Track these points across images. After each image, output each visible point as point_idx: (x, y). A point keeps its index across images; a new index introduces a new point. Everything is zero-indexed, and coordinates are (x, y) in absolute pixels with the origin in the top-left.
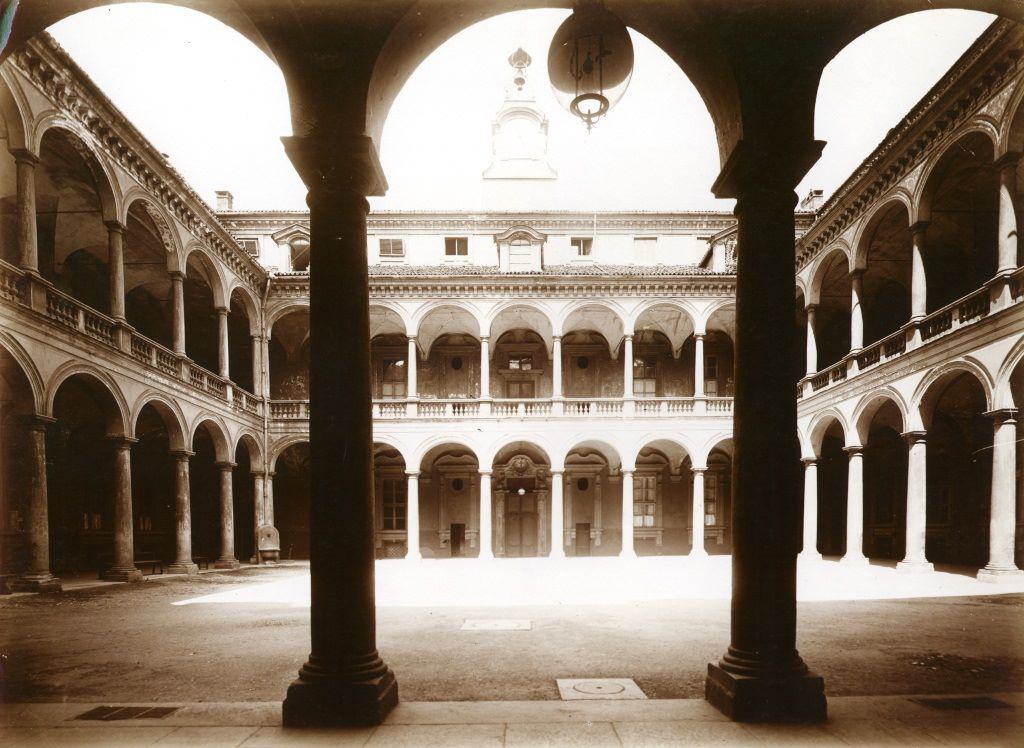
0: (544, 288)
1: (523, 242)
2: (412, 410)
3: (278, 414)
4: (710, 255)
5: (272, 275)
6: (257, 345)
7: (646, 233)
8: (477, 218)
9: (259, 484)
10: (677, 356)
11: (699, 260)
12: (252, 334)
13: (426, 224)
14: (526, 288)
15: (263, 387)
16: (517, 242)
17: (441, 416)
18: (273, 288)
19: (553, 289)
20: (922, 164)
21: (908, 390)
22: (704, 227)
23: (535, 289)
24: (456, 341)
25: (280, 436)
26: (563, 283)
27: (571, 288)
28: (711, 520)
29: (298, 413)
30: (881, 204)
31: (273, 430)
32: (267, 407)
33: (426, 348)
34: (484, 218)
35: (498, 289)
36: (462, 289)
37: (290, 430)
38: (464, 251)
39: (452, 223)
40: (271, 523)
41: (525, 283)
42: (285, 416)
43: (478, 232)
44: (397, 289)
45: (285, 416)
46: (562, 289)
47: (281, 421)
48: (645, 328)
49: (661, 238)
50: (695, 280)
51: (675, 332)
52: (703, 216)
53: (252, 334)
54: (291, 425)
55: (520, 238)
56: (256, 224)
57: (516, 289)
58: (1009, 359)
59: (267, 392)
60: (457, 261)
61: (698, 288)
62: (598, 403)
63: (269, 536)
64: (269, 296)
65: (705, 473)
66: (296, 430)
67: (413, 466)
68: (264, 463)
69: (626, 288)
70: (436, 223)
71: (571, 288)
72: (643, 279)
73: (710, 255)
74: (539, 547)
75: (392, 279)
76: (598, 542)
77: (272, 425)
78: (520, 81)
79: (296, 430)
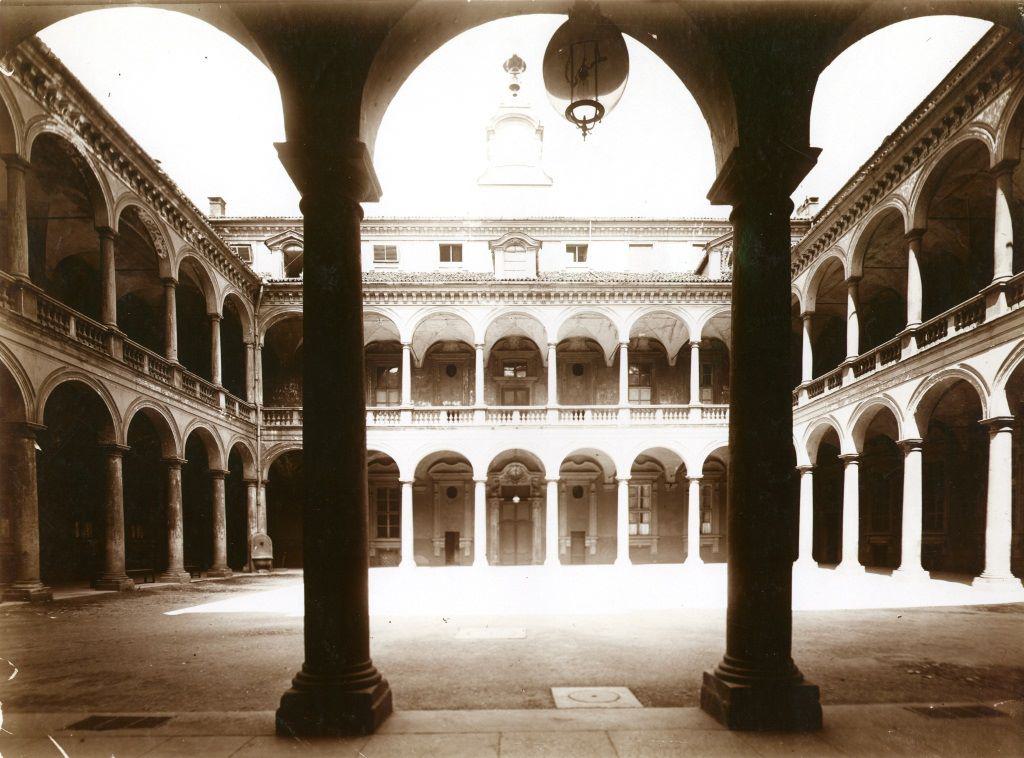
0: (539, 295)
1: (519, 248)
2: (406, 417)
3: (272, 421)
4: (706, 261)
5: (265, 282)
6: (250, 353)
7: (641, 239)
8: (472, 225)
9: (252, 492)
10: (672, 364)
11: (696, 266)
12: (245, 340)
13: (421, 230)
14: (521, 295)
15: (256, 396)
16: (512, 248)
17: (436, 424)
18: (266, 294)
19: (548, 296)
20: (918, 172)
21: (904, 398)
22: (700, 233)
23: (530, 296)
24: (451, 347)
25: (273, 444)
26: (558, 290)
27: (566, 295)
28: (707, 527)
29: (291, 421)
30: (876, 212)
31: (266, 438)
32: (260, 415)
33: (420, 355)
34: (479, 224)
35: (493, 295)
36: (457, 295)
37: (283, 438)
38: (458, 257)
39: (446, 229)
40: (263, 531)
41: (520, 290)
42: (278, 424)
43: (474, 239)
44: (391, 295)
45: (278, 424)
46: (557, 295)
47: (274, 428)
48: (640, 335)
49: (657, 245)
50: (691, 287)
51: (670, 340)
52: (699, 222)
53: (245, 340)
54: (284, 433)
55: (515, 245)
56: (249, 230)
57: (511, 295)
58: (1005, 367)
59: (260, 399)
60: (451, 267)
61: (693, 295)
62: (593, 410)
63: (262, 544)
64: (263, 302)
65: (701, 481)
66: (288, 438)
67: (407, 474)
68: (257, 471)
69: (621, 295)
70: (430, 229)
71: (566, 295)
72: (637, 287)
73: (706, 261)
74: (534, 557)
75: (386, 286)
76: (593, 551)
77: (265, 432)
78: (515, 87)
79: (288, 438)
